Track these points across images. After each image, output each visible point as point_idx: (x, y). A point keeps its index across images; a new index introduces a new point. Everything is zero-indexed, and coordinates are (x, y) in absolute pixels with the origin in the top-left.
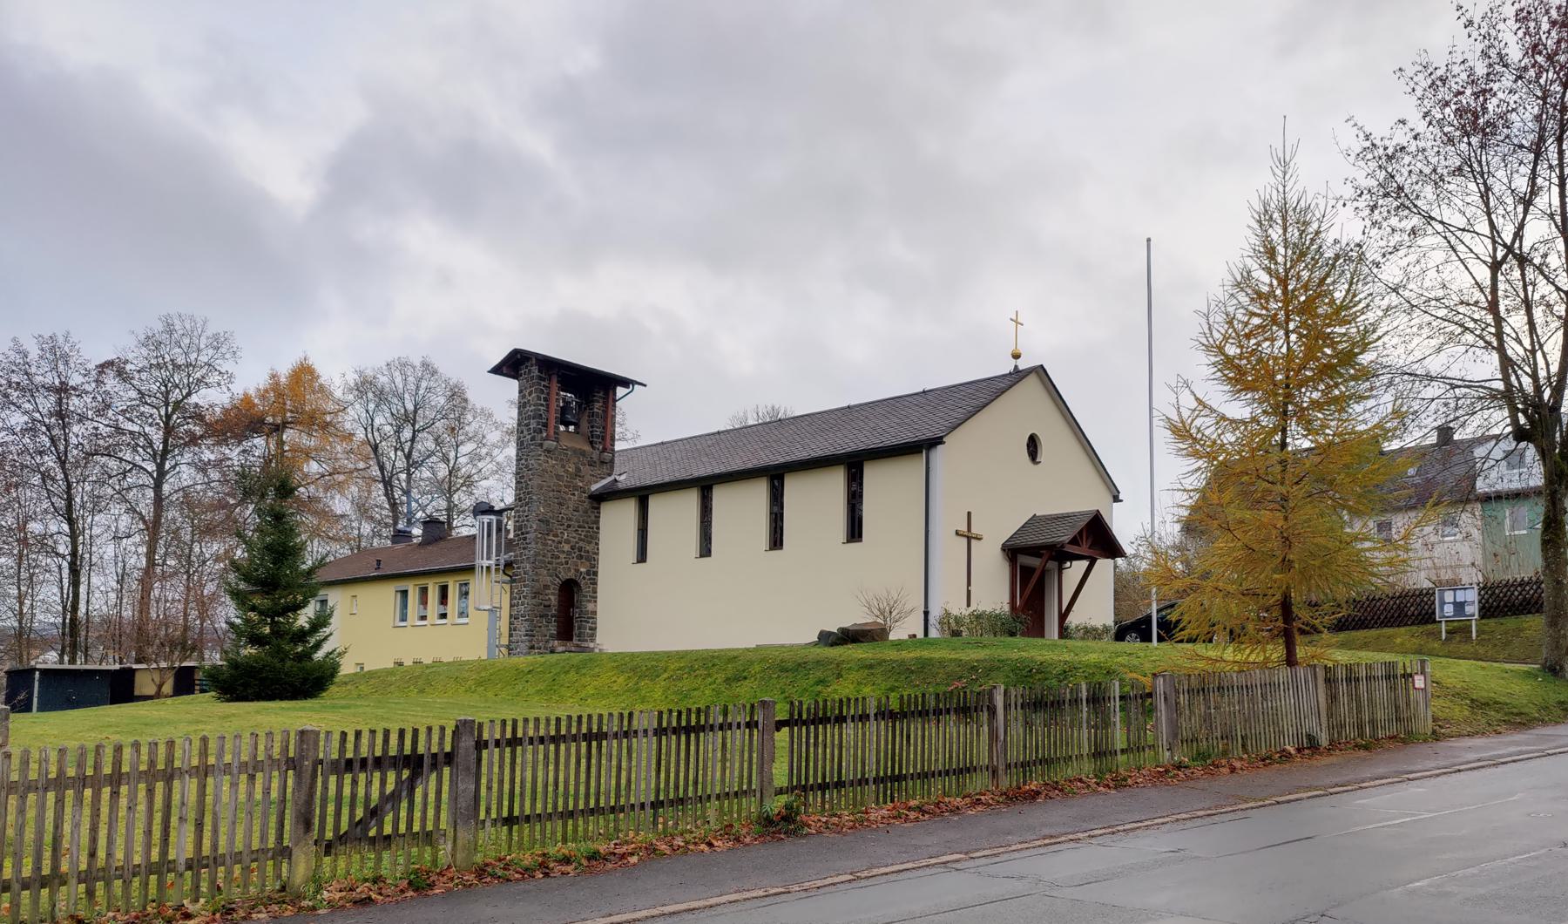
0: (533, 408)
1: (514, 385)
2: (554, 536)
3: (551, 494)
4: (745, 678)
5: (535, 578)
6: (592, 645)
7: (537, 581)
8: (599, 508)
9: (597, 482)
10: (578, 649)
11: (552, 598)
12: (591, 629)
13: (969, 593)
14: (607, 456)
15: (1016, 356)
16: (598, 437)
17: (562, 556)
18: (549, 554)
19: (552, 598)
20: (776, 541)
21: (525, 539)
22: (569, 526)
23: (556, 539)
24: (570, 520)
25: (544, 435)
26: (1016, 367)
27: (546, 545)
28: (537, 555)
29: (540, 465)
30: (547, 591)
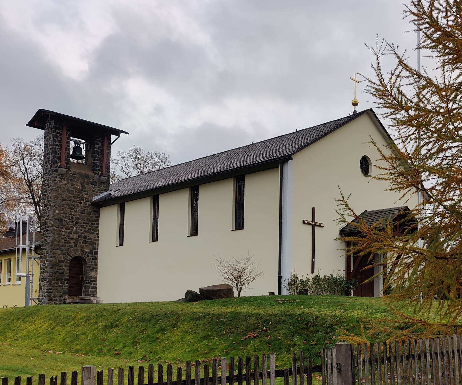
0: (51, 147)
1: (41, 133)
2: (66, 229)
3: (64, 202)
4: (116, 326)
6: (92, 298)
7: (54, 257)
8: (99, 212)
9: (97, 195)
10: (82, 301)
11: (65, 268)
12: (93, 288)
13: (313, 264)
14: (104, 178)
15: (355, 104)
17: (72, 242)
18: (63, 241)
19: (65, 268)
20: (194, 231)
21: (47, 231)
22: (77, 223)
23: (67, 231)
25: (59, 164)
26: (355, 111)
28: (53, 241)
29: (56, 183)
30: (62, 264)
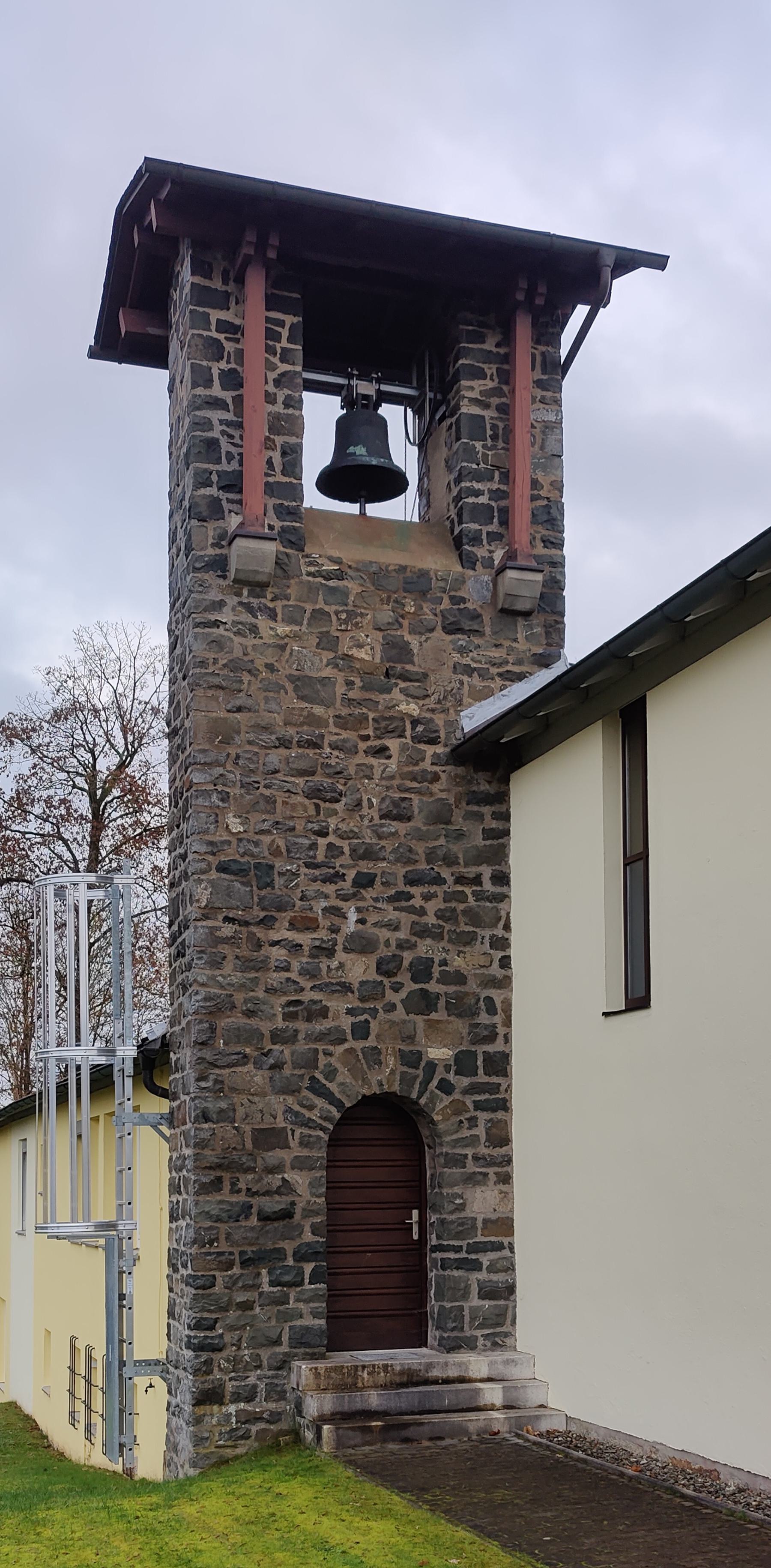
3: (274, 758)
5: (213, 1106)
7: (226, 1116)
8: (502, 797)
11: (299, 1180)
12: (488, 1293)
16: (483, 514)
17: (338, 1005)
18: (278, 1004)
19: (299, 1180)
22: (365, 881)
23: (305, 939)
24: (369, 854)
27: (262, 966)
30: (274, 1156)
